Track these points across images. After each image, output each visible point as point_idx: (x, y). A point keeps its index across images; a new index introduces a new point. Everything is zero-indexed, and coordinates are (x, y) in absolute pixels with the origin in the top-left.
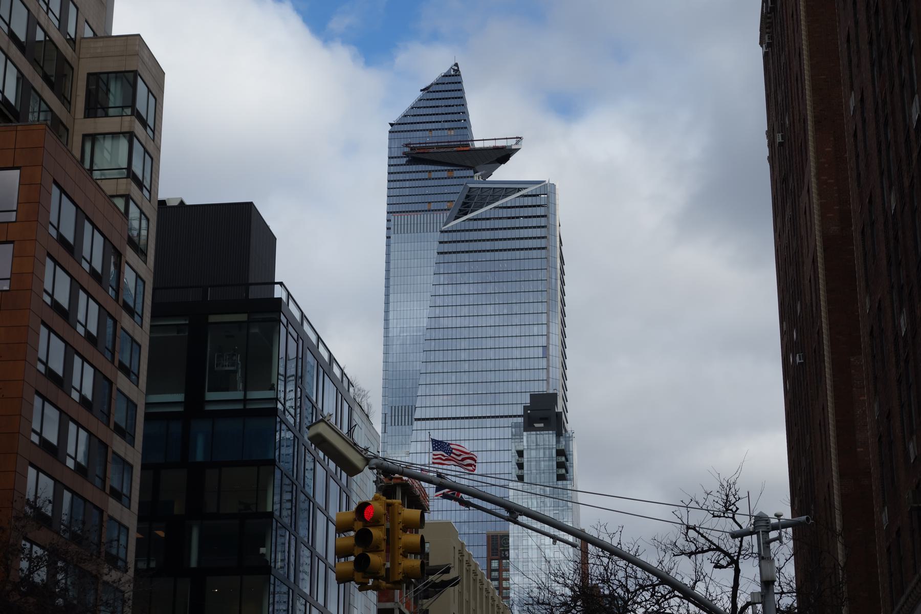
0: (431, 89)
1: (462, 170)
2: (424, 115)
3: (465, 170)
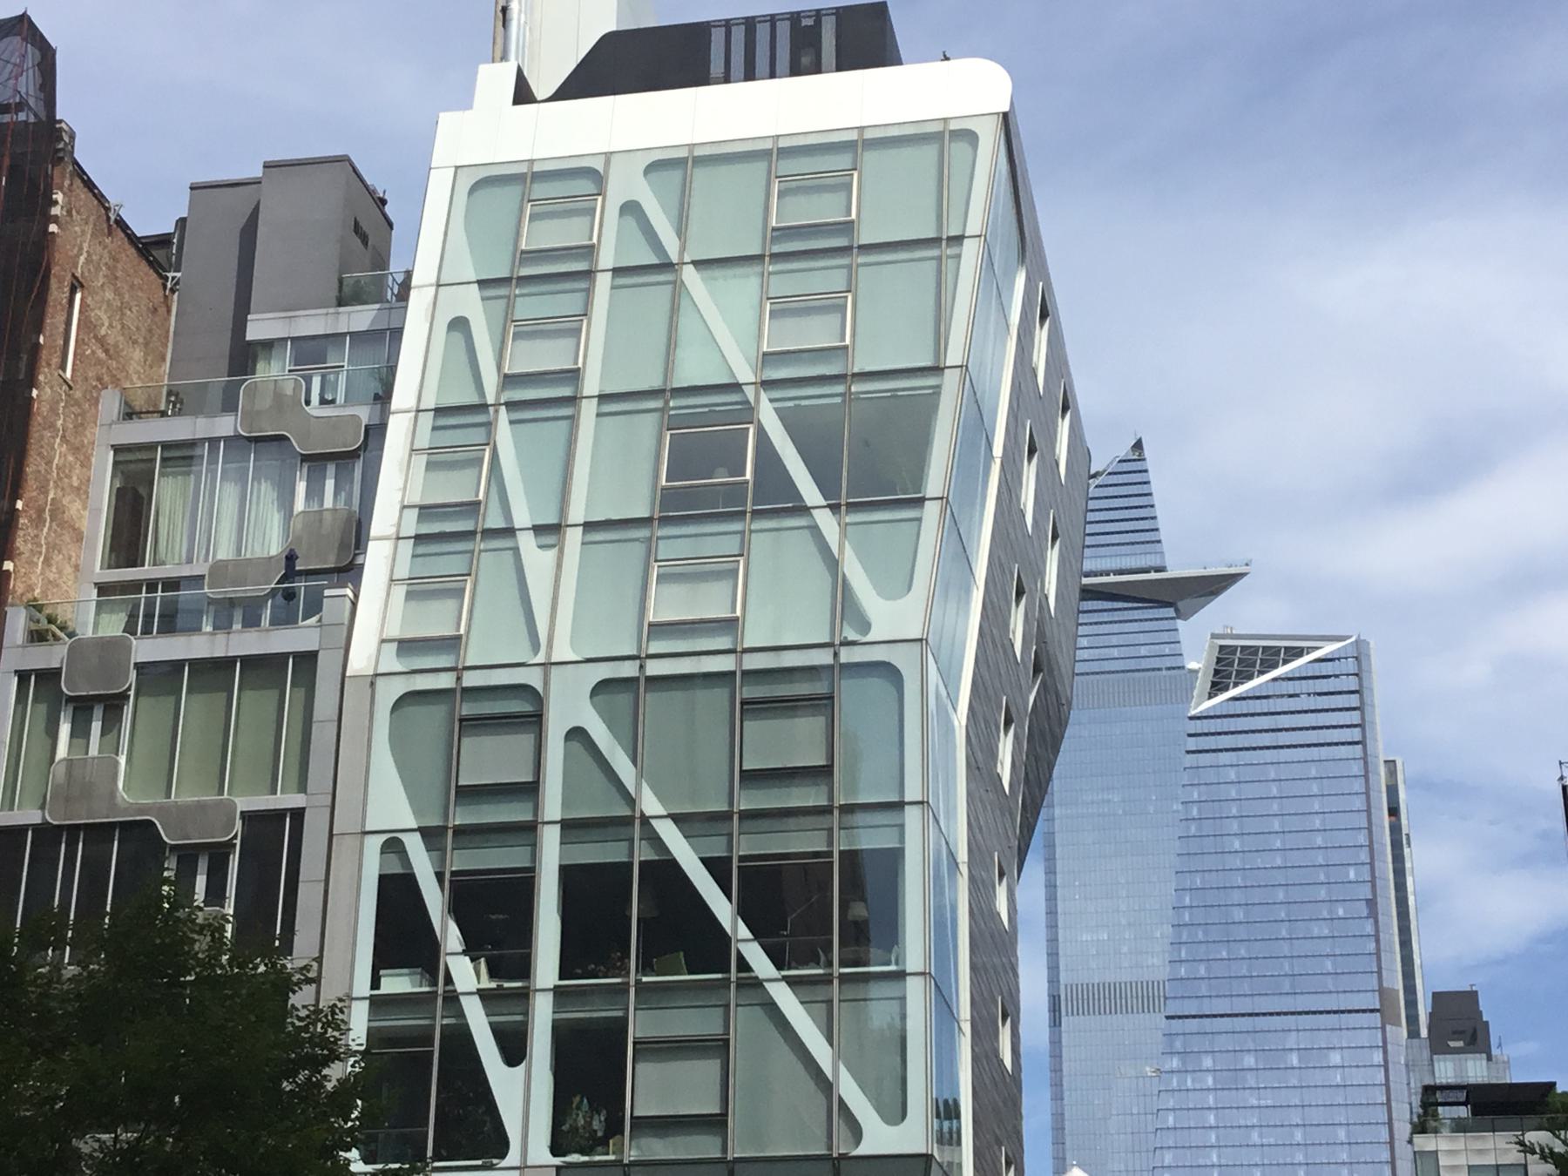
3: (1161, 607)
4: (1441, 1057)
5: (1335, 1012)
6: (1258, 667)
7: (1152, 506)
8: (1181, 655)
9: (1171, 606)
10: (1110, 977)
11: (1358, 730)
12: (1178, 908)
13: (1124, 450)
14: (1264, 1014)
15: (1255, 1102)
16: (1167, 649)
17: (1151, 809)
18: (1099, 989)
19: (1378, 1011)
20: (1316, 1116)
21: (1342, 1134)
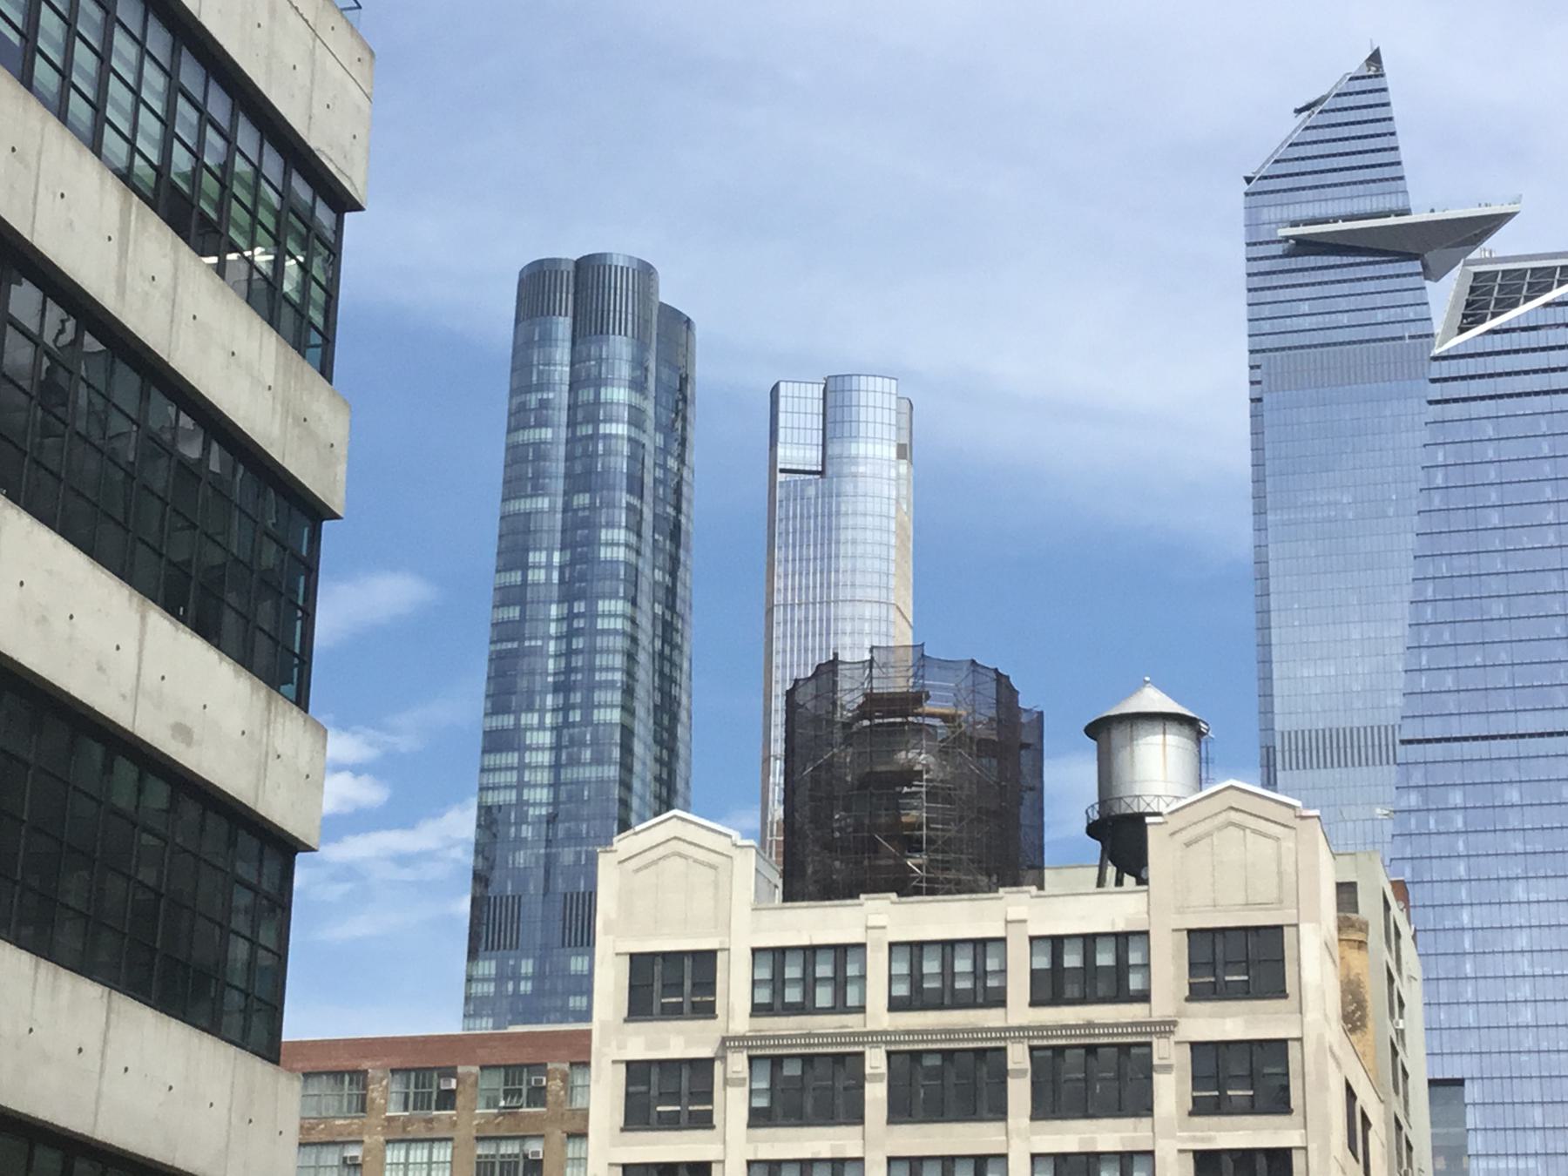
0: (1325, 106)
1: (1397, 261)
2: (1278, 191)
6: (1524, 292)
7: (1393, 134)
8: (1429, 319)
9: (1417, 259)
10: (1341, 721)
12: (1415, 602)
13: (1356, 64)
15: (1519, 847)
16: (1410, 313)
17: (1391, 511)
18: (1331, 736)
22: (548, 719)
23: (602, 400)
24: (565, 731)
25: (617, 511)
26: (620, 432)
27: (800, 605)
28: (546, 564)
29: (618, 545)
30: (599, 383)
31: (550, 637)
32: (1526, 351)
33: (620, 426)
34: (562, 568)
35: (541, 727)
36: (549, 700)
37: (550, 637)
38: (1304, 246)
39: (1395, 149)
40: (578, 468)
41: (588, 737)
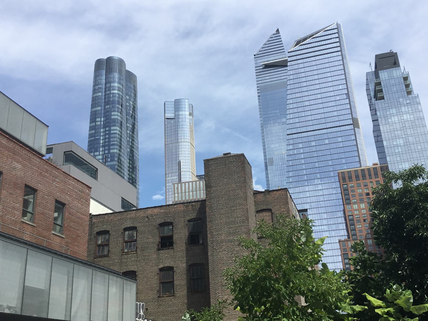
4: (382, 71)
5: (339, 126)
11: (339, 43)
13: (274, 32)
14: (317, 130)
19: (352, 124)
20: (336, 156)
21: (344, 161)
22: (101, 153)
23: (112, 86)
24: (104, 155)
25: (115, 108)
26: (116, 92)
27: (171, 144)
28: (100, 121)
29: (116, 115)
30: (110, 82)
31: (101, 136)
32: (309, 48)
33: (116, 91)
34: (104, 121)
35: (99, 155)
36: (101, 149)
37: (101, 136)
38: (267, 66)
39: (281, 38)
40: (107, 100)
41: (109, 156)
